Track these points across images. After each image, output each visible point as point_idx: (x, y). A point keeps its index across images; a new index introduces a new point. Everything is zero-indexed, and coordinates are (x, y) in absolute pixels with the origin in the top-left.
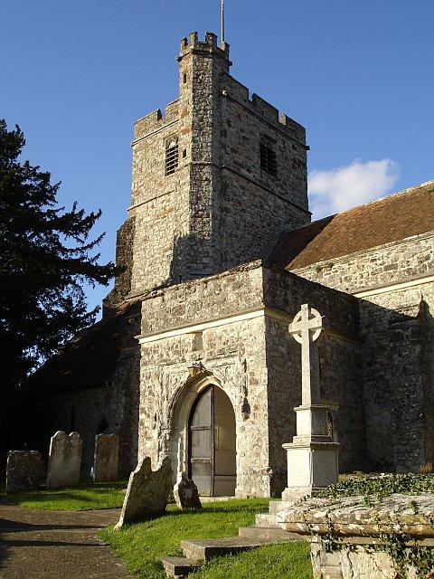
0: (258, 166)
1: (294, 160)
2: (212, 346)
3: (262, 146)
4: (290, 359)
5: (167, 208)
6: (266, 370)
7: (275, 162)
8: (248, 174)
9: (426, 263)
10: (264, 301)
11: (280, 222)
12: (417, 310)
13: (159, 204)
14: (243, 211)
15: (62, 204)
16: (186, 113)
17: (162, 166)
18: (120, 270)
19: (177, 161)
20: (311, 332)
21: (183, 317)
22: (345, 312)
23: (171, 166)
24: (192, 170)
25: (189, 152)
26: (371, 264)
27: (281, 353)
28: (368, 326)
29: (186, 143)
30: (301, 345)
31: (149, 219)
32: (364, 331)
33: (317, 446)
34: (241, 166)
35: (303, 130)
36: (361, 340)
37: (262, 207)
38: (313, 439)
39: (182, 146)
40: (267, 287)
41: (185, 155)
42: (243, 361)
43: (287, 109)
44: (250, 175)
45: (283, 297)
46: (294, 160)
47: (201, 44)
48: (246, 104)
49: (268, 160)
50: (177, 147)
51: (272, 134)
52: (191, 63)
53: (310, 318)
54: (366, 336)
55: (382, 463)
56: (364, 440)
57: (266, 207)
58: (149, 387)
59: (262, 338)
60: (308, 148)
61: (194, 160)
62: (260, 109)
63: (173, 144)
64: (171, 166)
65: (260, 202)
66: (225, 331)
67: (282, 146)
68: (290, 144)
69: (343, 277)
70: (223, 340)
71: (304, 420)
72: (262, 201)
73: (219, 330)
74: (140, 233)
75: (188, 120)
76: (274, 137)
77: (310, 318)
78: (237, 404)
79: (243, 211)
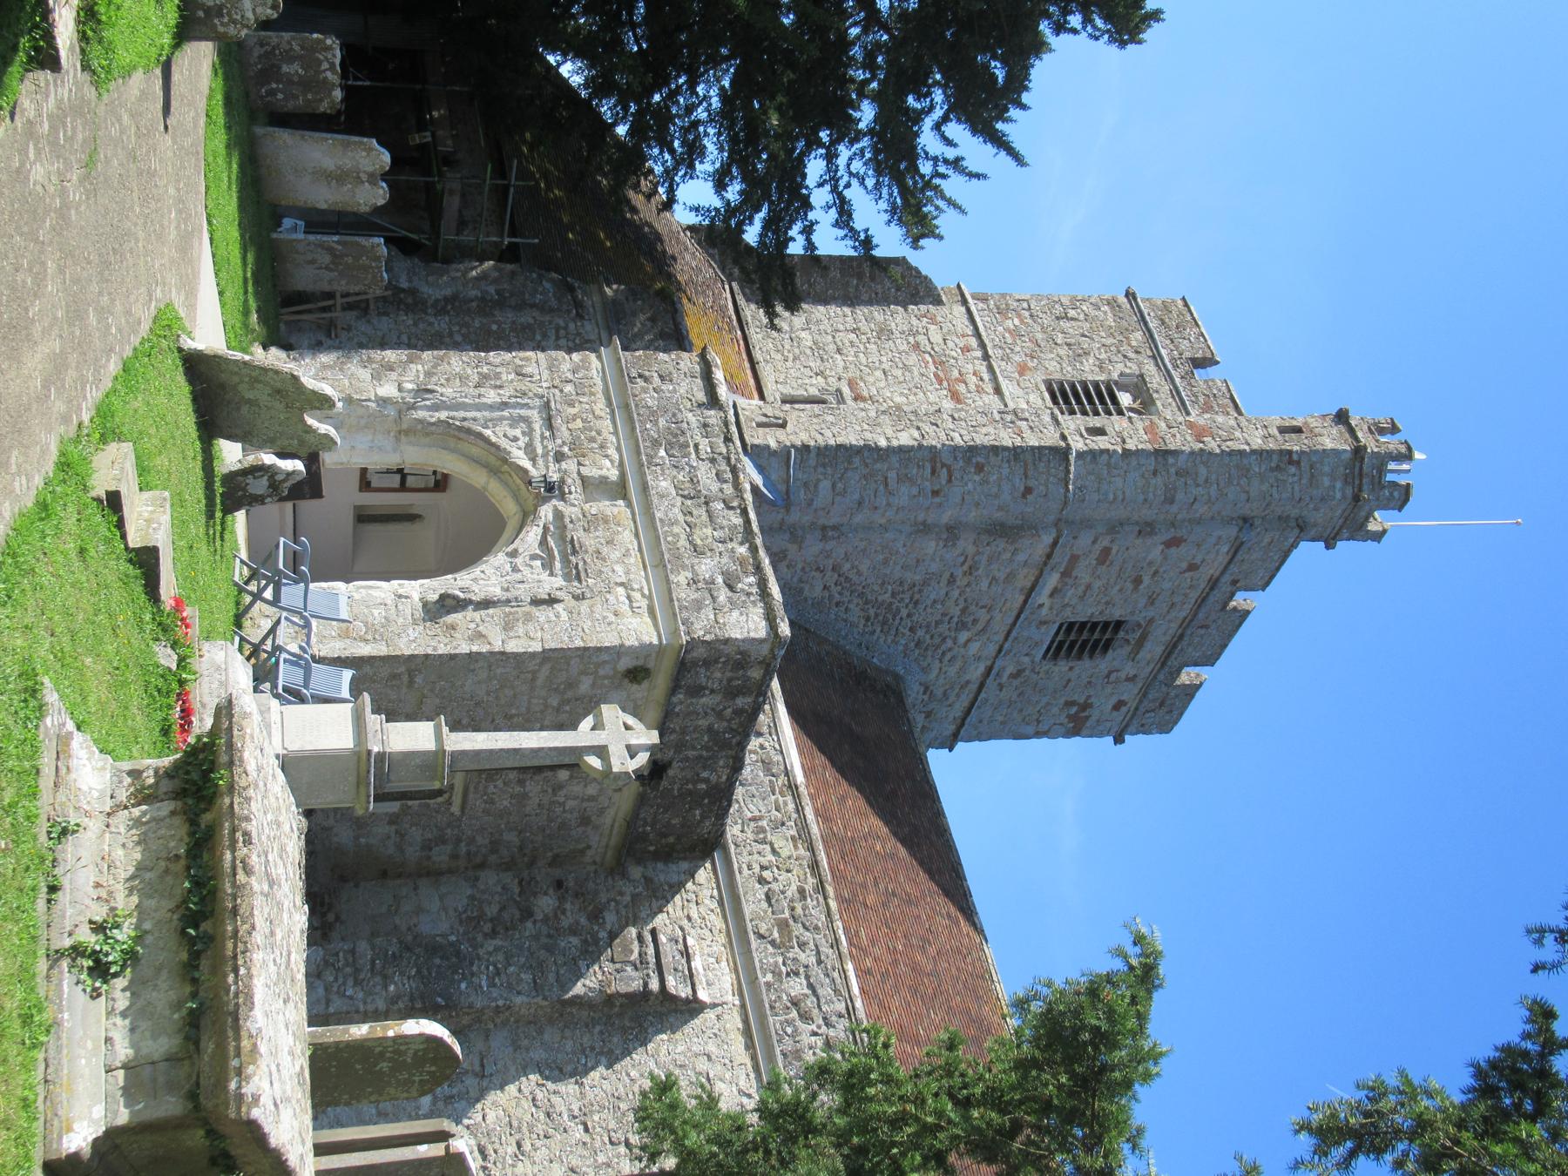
0: (1069, 616)
1: (1086, 706)
2: (592, 522)
3: (1119, 624)
4: (564, 702)
5: (961, 388)
6: (536, 647)
7: (1079, 657)
8: (1047, 591)
9: (794, 1014)
10: (693, 644)
11: (925, 670)
12: (684, 992)
13: (973, 365)
14: (952, 580)
15: (941, 138)
16: (1199, 434)
17: (1070, 373)
18: (777, 281)
19: (1072, 412)
20: (601, 751)
21: (662, 453)
22: (676, 820)
23: (1066, 396)
24: (1054, 450)
25: (1101, 443)
26: (794, 888)
27: (564, 683)
28: (648, 881)
29: (1126, 432)
30: (575, 728)
31: (936, 337)
32: (636, 872)
33: (430, 762)
34: (1066, 574)
35: (1166, 727)
36: (617, 869)
37: (962, 626)
38: (381, 757)
39: (1116, 424)
40: (727, 649)
41: (1100, 432)
42: (559, 594)
43: (1219, 686)
44: (1042, 597)
45: (701, 696)
46: (1086, 706)
47: (1382, 470)
48: (1224, 586)
49: (1084, 639)
50: (1120, 413)
51: (1153, 649)
52: (1328, 444)
53: (628, 747)
54: (624, 875)
55: (331, 917)
56: (384, 874)
57: (963, 636)
58: (498, 376)
59: (609, 640)
60: (1119, 740)
61: (1080, 455)
62: (1209, 628)
63: (1125, 399)
64: (1066, 396)
65: (975, 621)
66: (626, 554)
67: (1123, 675)
68: (1129, 693)
69: (764, 823)
70: (605, 550)
71: (413, 737)
72: (979, 626)
73: (620, 554)
74: (898, 318)
75: (1181, 441)
76: (1144, 654)
77: (628, 747)
78: (460, 583)
79: (952, 580)
